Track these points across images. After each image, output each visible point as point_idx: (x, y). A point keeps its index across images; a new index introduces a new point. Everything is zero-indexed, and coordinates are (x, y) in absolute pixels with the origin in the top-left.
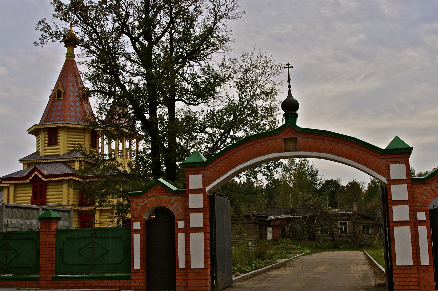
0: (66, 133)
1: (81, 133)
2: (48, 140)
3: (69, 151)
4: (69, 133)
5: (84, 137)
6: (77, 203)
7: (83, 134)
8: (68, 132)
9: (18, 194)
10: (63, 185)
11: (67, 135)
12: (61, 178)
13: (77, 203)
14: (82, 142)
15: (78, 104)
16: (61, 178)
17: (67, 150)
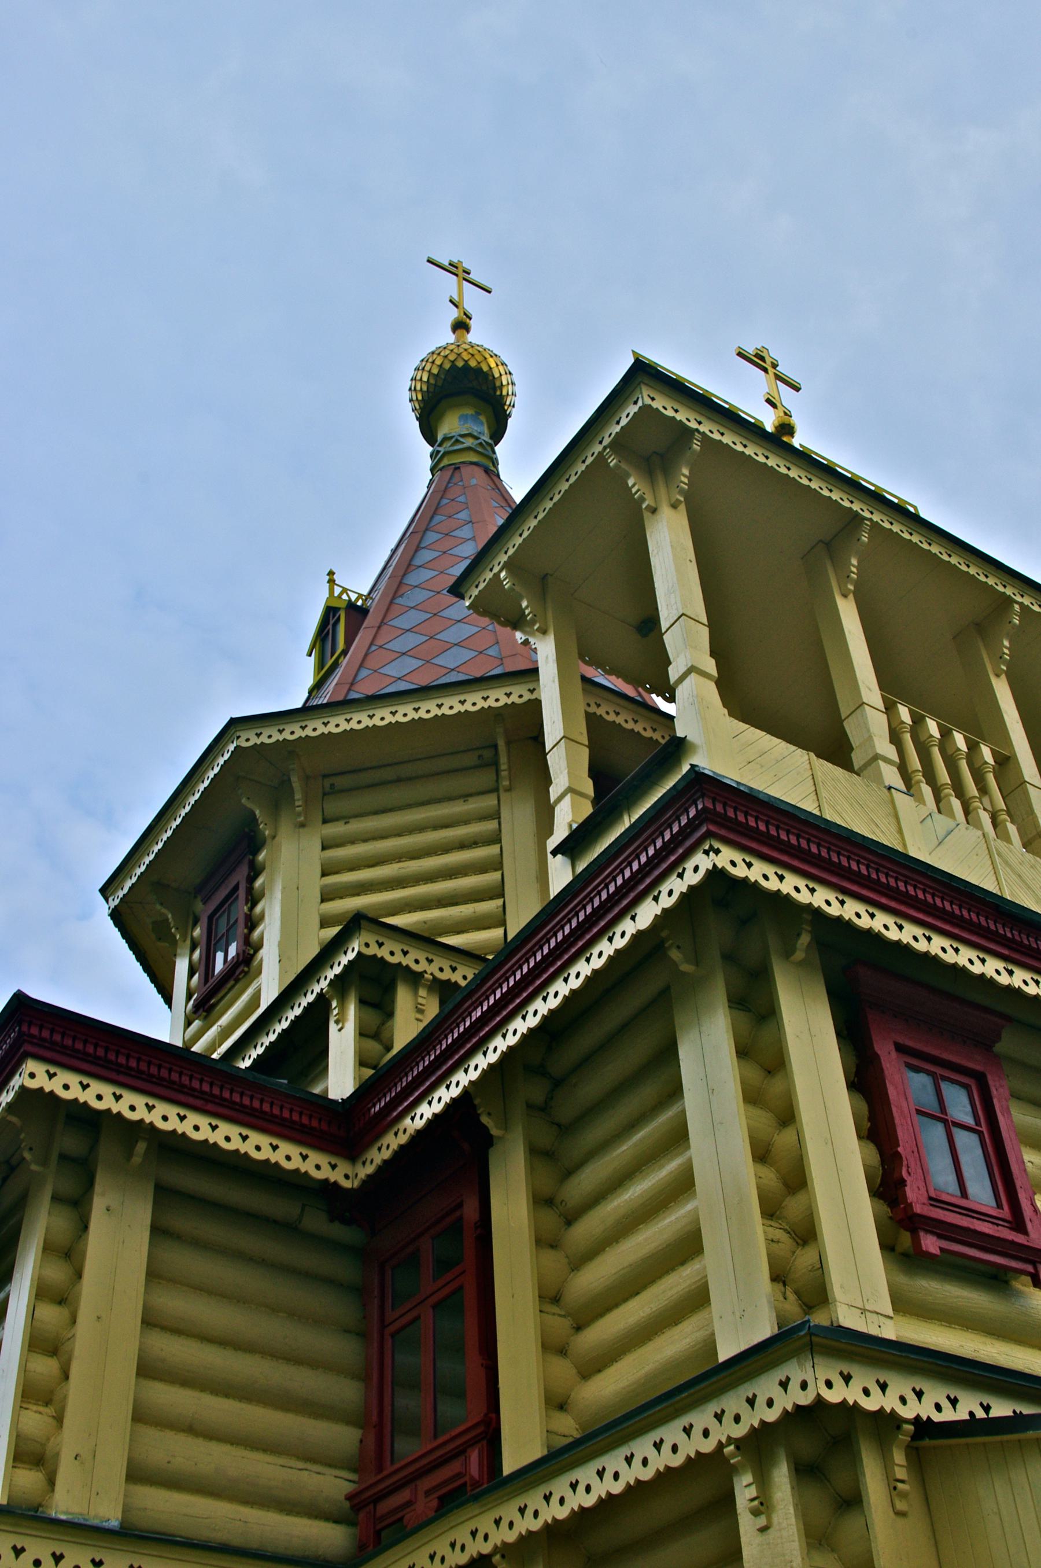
14: (481, 868)
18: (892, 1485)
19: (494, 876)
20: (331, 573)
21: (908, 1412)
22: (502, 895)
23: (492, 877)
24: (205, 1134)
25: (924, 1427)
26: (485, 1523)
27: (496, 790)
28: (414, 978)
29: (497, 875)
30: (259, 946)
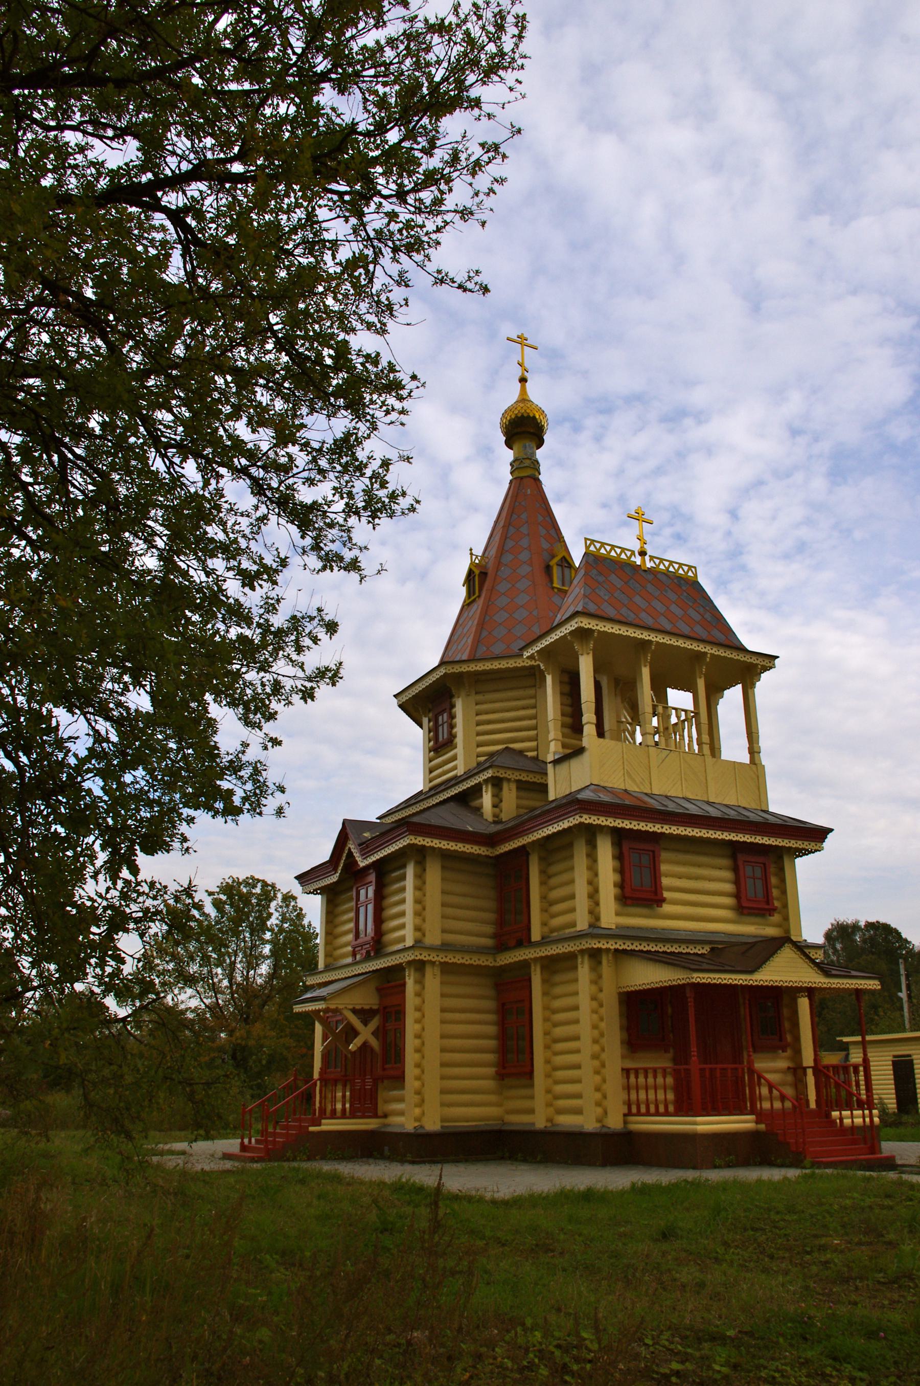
0: (474, 698)
1: (525, 688)
2: (853, 1128)
3: (482, 759)
4: (480, 697)
5: (532, 701)
6: (489, 942)
7: (531, 692)
8: (476, 693)
9: (555, 875)
10: (442, 1127)
11: (477, 704)
12: (657, 828)
13: (489, 942)
14: (530, 739)
15: (505, 572)
16: (657, 828)
17: (478, 756)
18: (608, 961)
19: (534, 722)
20: (471, 550)
21: (612, 948)
22: (537, 740)
23: (533, 722)
24: (454, 848)
25: (616, 950)
26: (527, 952)
27: (535, 686)
28: (509, 780)
29: (535, 732)
30: (455, 737)
